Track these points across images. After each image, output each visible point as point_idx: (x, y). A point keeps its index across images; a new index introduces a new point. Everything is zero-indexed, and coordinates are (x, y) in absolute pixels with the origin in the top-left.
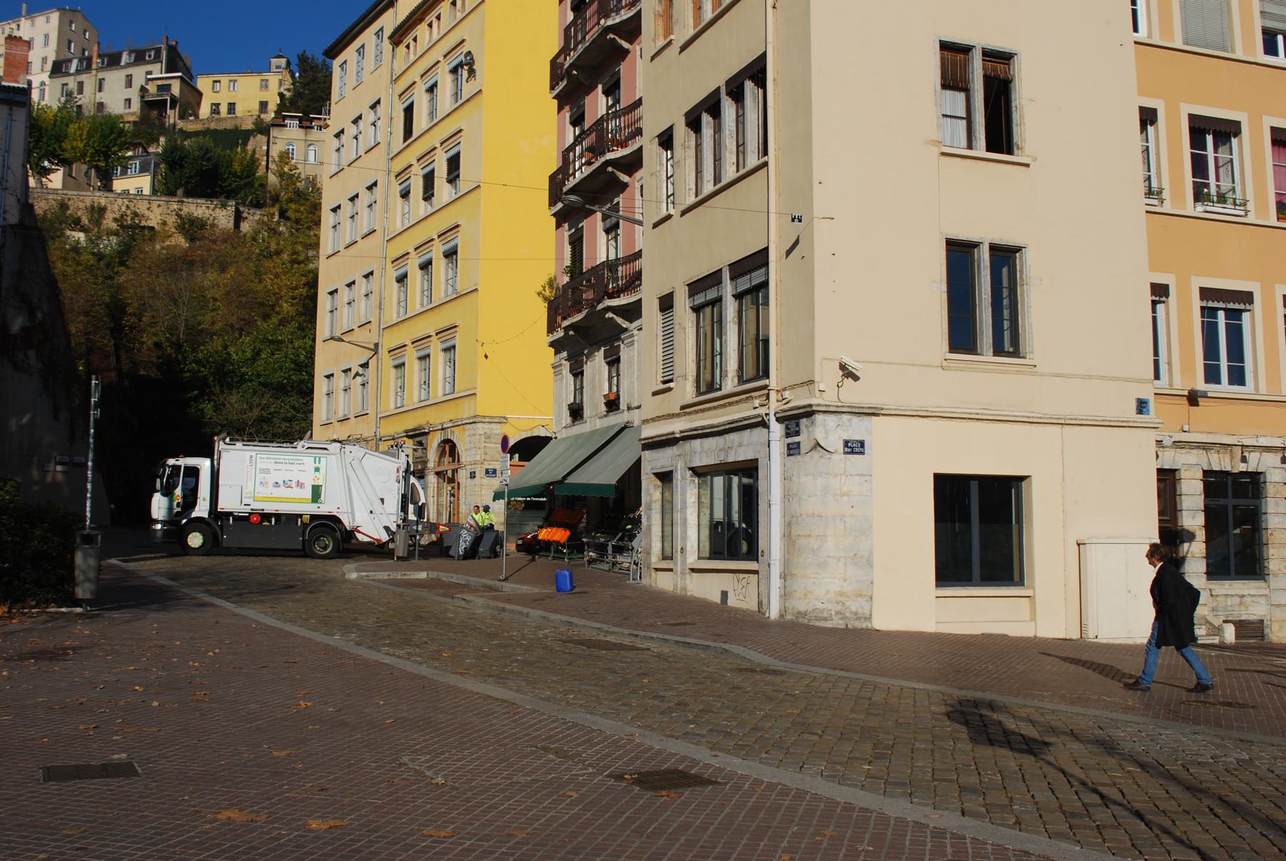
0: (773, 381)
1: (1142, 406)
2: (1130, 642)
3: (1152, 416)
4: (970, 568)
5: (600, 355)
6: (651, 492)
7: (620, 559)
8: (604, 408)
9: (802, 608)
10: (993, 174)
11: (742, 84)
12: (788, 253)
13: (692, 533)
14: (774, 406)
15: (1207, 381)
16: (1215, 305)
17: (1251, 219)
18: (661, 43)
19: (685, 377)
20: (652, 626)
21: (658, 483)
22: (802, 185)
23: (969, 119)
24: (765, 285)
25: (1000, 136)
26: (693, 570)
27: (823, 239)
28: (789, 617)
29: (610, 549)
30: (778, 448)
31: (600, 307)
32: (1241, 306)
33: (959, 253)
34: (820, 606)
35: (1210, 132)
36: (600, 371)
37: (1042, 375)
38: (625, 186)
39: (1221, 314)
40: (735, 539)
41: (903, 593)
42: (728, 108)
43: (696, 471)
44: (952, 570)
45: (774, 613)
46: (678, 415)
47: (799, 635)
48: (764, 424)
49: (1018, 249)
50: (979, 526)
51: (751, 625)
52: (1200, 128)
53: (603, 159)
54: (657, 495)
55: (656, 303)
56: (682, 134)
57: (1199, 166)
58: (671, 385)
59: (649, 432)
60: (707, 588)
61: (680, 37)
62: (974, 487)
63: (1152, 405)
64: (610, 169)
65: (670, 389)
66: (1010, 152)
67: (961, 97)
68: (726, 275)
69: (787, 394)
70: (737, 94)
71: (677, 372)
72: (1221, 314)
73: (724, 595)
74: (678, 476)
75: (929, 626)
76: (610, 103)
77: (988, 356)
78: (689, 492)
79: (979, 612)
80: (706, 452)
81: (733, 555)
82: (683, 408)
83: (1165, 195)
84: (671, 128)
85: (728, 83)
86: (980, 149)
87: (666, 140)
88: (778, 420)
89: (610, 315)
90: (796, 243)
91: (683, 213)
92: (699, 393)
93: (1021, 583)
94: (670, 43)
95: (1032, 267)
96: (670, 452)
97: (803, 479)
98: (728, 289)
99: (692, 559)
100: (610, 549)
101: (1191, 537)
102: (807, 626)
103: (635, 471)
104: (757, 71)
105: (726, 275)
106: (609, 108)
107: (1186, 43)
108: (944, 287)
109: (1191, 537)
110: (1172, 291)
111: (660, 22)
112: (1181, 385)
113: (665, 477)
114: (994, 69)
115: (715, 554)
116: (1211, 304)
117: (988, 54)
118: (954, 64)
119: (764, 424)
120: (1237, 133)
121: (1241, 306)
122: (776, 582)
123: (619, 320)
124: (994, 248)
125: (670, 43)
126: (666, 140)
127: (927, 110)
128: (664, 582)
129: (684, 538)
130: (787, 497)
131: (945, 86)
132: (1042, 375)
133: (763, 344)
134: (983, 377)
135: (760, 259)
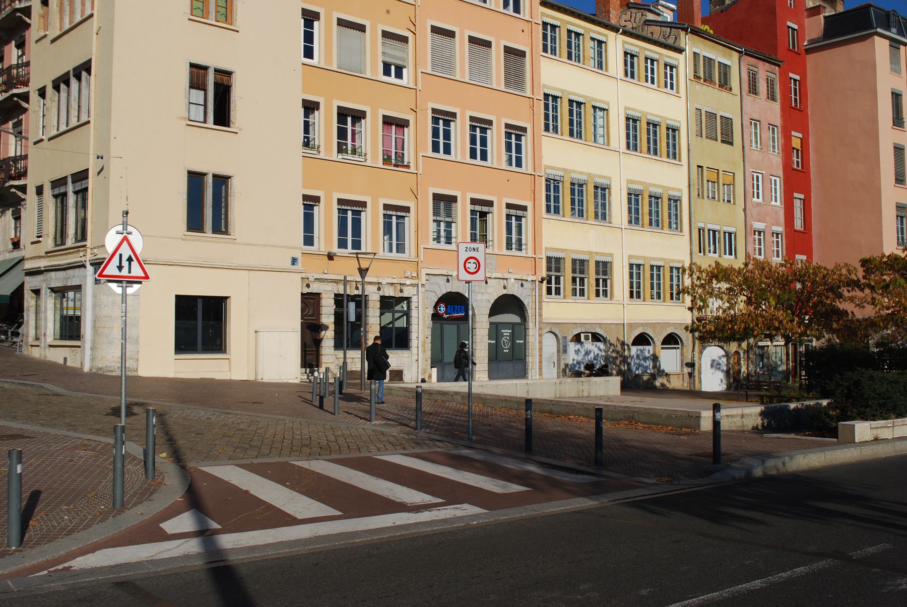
0: (88, 243)
1: (294, 261)
2: (280, 381)
3: (299, 266)
4: (196, 345)
5: (9, 213)
6: (29, 301)
7: (15, 339)
8: (11, 246)
9: (100, 366)
10: (219, 135)
11: (80, 73)
12: (99, 173)
13: (50, 325)
14: (89, 257)
15: (339, 247)
16: (346, 208)
17: (368, 163)
18: (42, 34)
19: (48, 235)
20: (13, 377)
21: (34, 295)
22: (105, 139)
23: (205, 106)
24: (86, 189)
25: (222, 117)
26: (50, 346)
27: (115, 168)
28: (94, 371)
29: (9, 333)
30: (90, 281)
31: (7, 185)
32: (360, 209)
33: (195, 179)
34: (109, 364)
35: (349, 117)
36: (9, 224)
37: (240, 244)
38: (26, 110)
39: (350, 213)
40: (71, 328)
41: (156, 356)
42: (74, 82)
43: (53, 290)
44: (185, 343)
45: (86, 369)
46: (43, 257)
47: (99, 380)
48: (84, 266)
49: (229, 177)
50: (201, 322)
51: (76, 373)
52: (343, 114)
53: (11, 93)
54: (33, 302)
55: (34, 189)
56: (50, 91)
57: (342, 134)
58: (40, 239)
59: (28, 265)
60: (56, 356)
61: (54, 32)
62: (200, 302)
63: (300, 261)
64: (15, 99)
65: (39, 242)
66: (229, 126)
67: (202, 93)
68: (70, 180)
69: (95, 251)
70: (78, 77)
71: (44, 232)
72: (350, 213)
73: (65, 359)
74: (43, 292)
75: (170, 374)
76: (20, 53)
77: (209, 233)
78: (49, 301)
79: (200, 367)
80: (57, 279)
81: (71, 338)
82: (47, 253)
83: (322, 149)
84: (45, 87)
85: (74, 69)
86: (210, 122)
87: (42, 93)
88: (91, 264)
89: (13, 190)
90: (102, 169)
91: (50, 139)
92: (56, 245)
93: (225, 352)
94: (45, 36)
95: (236, 187)
96: (39, 278)
97: (102, 297)
98: (70, 188)
99: (50, 340)
100: (9, 333)
101: (326, 328)
102: (102, 375)
103: (21, 287)
104: (86, 67)
105: (70, 180)
106: (19, 57)
107: (339, 67)
108: (185, 196)
109: (326, 328)
110: (322, 200)
111: (42, 20)
112: (324, 250)
113: (37, 292)
114: (222, 79)
115: (62, 337)
116: (343, 207)
117: (217, 71)
118: (198, 76)
119: (84, 266)
120: (364, 117)
121: (360, 209)
122: (88, 352)
123: (20, 194)
124: (215, 176)
125: (45, 36)
126: (42, 93)
127: (179, 98)
128: (36, 353)
129: (46, 328)
130: (95, 306)
131: (192, 87)
132: (240, 244)
133: (84, 220)
134: (206, 244)
135: (82, 176)
